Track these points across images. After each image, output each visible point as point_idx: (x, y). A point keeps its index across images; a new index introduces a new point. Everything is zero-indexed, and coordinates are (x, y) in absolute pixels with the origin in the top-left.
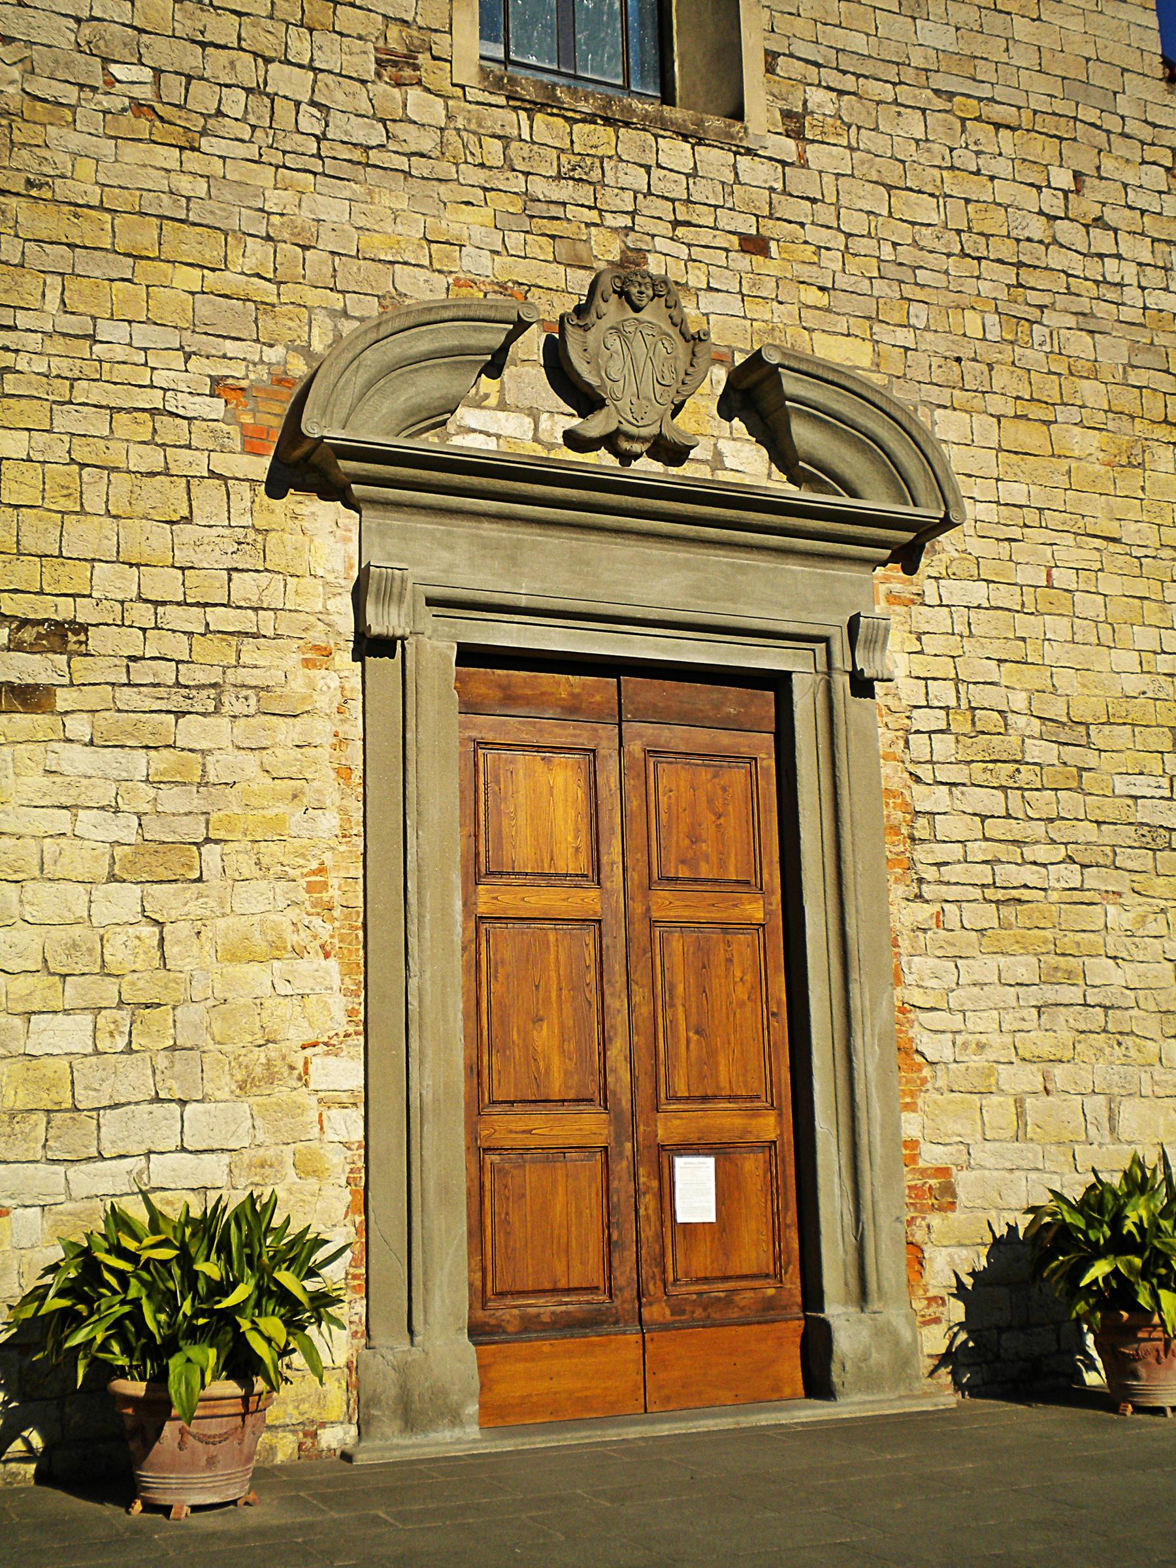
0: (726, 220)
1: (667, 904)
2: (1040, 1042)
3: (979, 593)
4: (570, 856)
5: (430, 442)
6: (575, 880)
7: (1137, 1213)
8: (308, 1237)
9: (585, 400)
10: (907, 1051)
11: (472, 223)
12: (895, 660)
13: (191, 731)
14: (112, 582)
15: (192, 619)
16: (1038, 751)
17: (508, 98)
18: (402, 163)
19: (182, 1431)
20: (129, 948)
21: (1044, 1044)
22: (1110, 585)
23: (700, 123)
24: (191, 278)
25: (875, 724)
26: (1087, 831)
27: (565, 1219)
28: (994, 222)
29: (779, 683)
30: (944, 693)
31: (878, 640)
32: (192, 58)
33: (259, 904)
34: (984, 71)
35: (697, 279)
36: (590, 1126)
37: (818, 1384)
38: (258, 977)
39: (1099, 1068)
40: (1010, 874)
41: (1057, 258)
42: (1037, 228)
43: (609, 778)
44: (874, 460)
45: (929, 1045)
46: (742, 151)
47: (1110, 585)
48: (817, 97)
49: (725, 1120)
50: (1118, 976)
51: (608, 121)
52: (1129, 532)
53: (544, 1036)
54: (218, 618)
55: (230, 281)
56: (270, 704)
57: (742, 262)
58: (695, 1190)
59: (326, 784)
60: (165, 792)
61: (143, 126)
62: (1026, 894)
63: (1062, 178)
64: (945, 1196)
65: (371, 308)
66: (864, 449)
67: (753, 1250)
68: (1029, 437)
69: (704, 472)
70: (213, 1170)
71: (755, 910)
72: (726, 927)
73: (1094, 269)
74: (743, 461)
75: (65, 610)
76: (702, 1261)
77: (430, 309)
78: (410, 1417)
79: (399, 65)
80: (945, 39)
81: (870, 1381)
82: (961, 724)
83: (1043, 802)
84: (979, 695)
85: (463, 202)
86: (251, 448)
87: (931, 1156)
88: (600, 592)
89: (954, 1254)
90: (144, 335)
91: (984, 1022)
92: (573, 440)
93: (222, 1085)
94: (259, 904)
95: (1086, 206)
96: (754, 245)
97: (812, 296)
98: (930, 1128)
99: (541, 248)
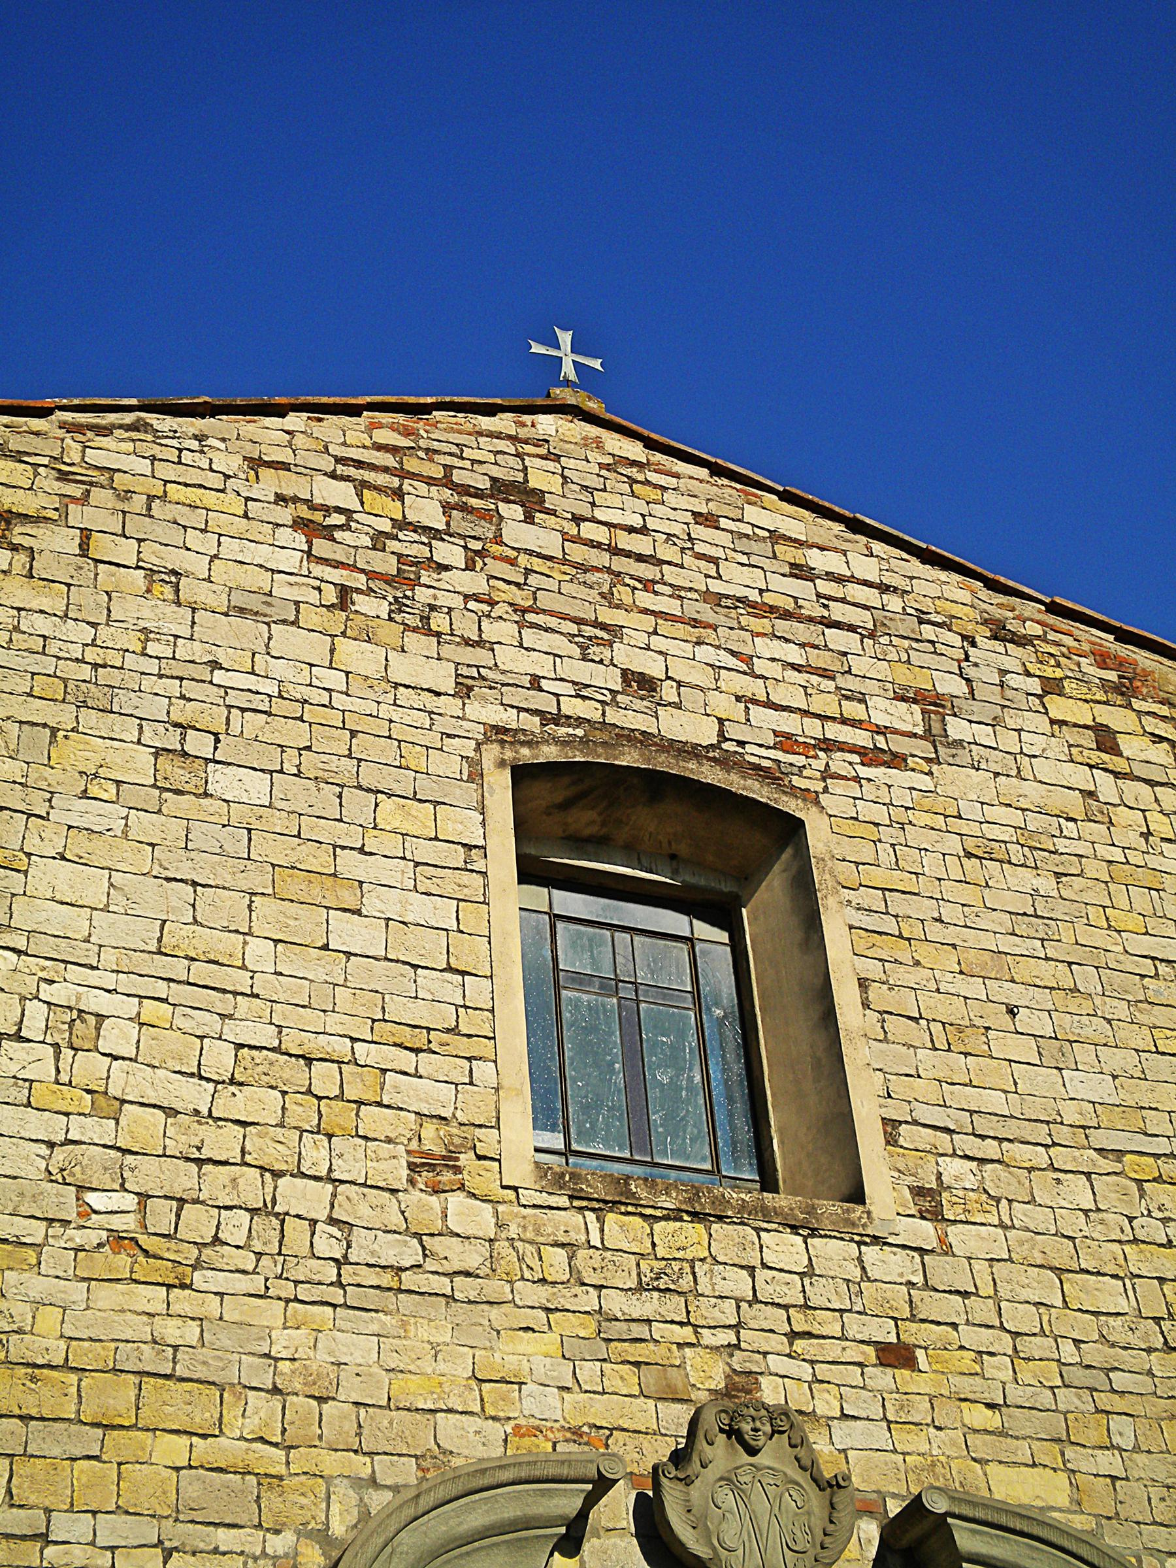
11: (534, 1354)
17: (571, 1197)
24: (175, 1449)
32: (184, 1178)
46: (867, 1240)
48: (953, 1168)
55: (225, 1449)
57: (882, 1378)
65: (407, 1472)
77: (483, 1471)
79: (435, 1168)
80: (1103, 1089)
85: (521, 1329)
90: (111, 1529)
96: (897, 1355)
97: (979, 1416)
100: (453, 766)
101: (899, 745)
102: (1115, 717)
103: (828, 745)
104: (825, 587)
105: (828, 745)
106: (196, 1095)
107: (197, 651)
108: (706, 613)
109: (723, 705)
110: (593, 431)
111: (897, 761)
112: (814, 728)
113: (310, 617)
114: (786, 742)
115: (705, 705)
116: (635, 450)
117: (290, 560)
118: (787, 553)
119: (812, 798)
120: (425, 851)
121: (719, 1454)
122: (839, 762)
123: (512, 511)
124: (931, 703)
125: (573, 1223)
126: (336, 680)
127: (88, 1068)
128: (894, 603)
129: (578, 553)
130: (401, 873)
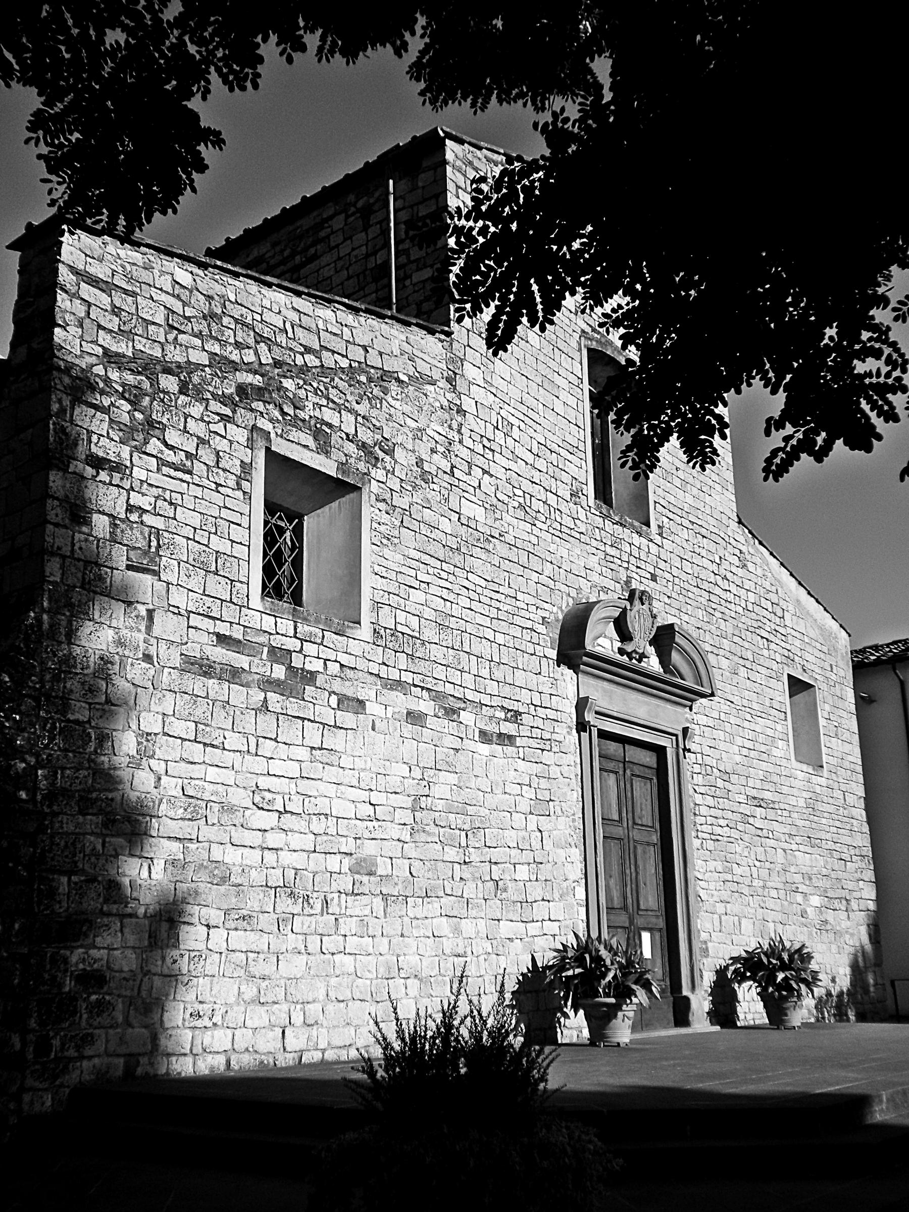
13: (547, 757)
18: (578, 536)
19: (624, 1015)
23: (641, 528)
44: (692, 668)
51: (621, 524)
52: (735, 699)
60: (542, 780)
62: (720, 838)
66: (690, 664)
69: (645, 665)
74: (653, 664)
88: (630, 712)
92: (621, 651)
100: (575, 345)
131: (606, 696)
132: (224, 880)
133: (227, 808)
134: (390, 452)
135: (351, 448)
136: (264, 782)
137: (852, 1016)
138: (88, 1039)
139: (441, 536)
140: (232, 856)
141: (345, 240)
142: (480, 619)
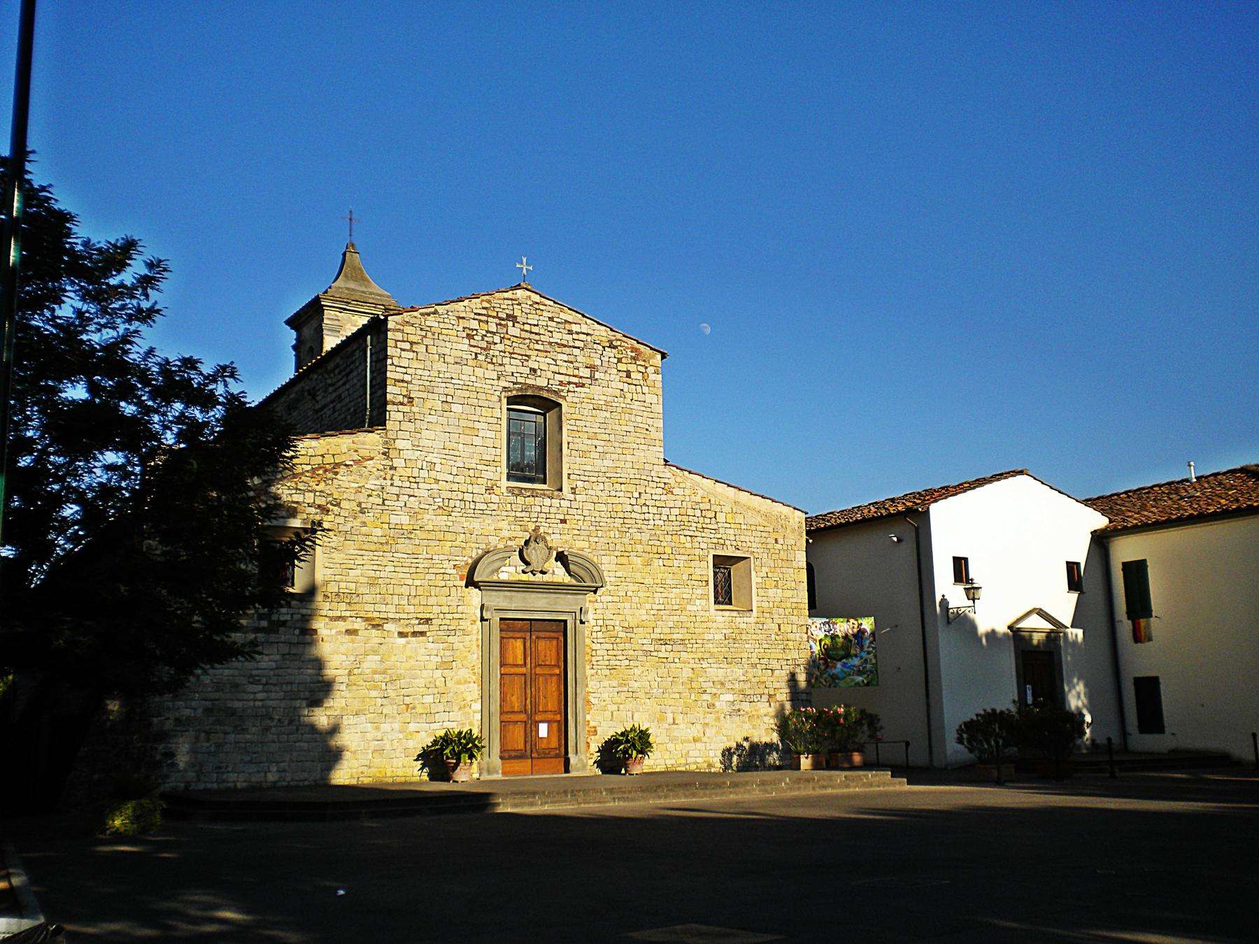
0: (558, 516)
1: (538, 670)
2: (617, 699)
3: (610, 599)
4: (520, 662)
5: (495, 578)
6: (521, 666)
7: (631, 735)
8: (787, 713)
9: (527, 563)
10: (588, 701)
11: (504, 525)
12: (590, 617)
14: (436, 609)
15: (450, 616)
16: (622, 634)
20: (440, 682)
21: (619, 700)
22: (640, 594)
24: (449, 544)
25: (586, 630)
26: (631, 652)
27: (517, 738)
28: (619, 508)
29: (565, 621)
30: (600, 622)
31: (587, 612)
32: (449, 495)
33: (463, 673)
34: (619, 470)
35: (550, 531)
36: (523, 717)
37: (567, 770)
38: (462, 687)
39: (630, 705)
40: (612, 663)
41: (633, 515)
42: (629, 508)
43: (528, 644)
45: (592, 700)
47: (640, 594)
48: (579, 483)
49: (550, 716)
50: (636, 685)
53: (514, 698)
54: (456, 616)
55: (457, 543)
56: (465, 633)
57: (560, 526)
58: (543, 730)
59: (474, 648)
61: (440, 511)
63: (636, 495)
64: (595, 733)
65: (484, 546)
67: (554, 744)
68: (624, 560)
70: (454, 725)
71: (557, 671)
72: (551, 675)
73: (642, 517)
75: (428, 616)
76: (544, 746)
78: (489, 772)
79: (489, 489)
80: (610, 464)
81: (578, 770)
82: (604, 629)
83: (621, 646)
84: (608, 622)
86: (461, 579)
87: (592, 724)
89: (595, 745)
90: (442, 557)
91: (605, 696)
93: (456, 708)
94: (463, 673)
95: (641, 501)
96: (563, 521)
97: (576, 532)
98: (593, 718)
99: (518, 528)
100: (497, 399)
101: (584, 381)
102: (632, 368)
103: (569, 383)
104: (575, 336)
105: (569, 383)
106: (450, 478)
107: (447, 375)
108: (548, 348)
109: (550, 375)
110: (529, 293)
111: (583, 385)
112: (567, 379)
113: (470, 363)
114: (561, 383)
115: (546, 374)
116: (537, 298)
117: (466, 347)
118: (568, 326)
119: (564, 398)
120: (490, 420)
121: (532, 544)
122: (572, 387)
123: (510, 324)
124: (592, 368)
125: (512, 499)
126: (474, 379)
127: (433, 474)
128: (589, 338)
129: (524, 335)
130: (485, 426)
131: (497, 599)
132: (233, 714)
133: (236, 686)
134: (338, 505)
135: (313, 510)
136: (254, 672)
137: (805, 762)
138: (167, 776)
139: (376, 539)
140: (237, 705)
141: (196, 368)
142: (401, 575)
